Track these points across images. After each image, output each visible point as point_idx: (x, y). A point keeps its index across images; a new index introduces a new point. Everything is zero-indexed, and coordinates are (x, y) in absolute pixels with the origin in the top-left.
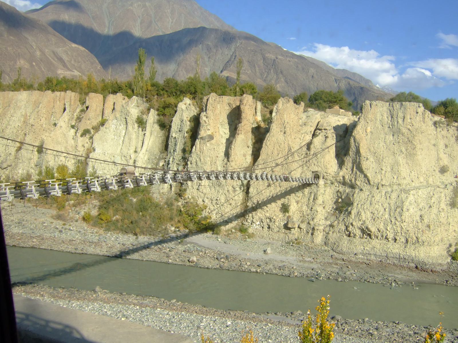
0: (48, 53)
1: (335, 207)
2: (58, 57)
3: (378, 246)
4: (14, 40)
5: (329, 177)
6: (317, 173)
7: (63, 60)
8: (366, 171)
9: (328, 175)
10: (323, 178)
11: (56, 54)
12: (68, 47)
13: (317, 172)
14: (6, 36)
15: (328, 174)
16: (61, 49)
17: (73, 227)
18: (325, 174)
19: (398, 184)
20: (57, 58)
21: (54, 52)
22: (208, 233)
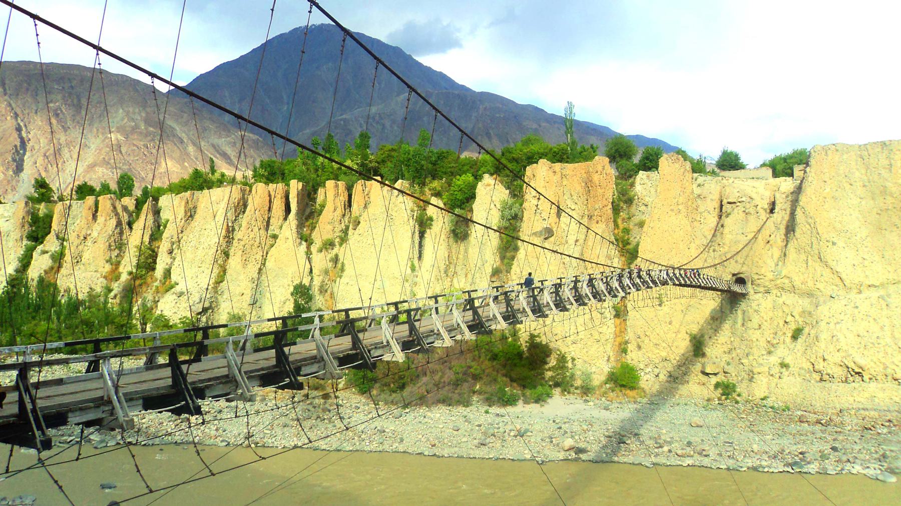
0: (205, 147)
1: (370, 503)
2: (221, 152)
3: (880, 395)
4: (155, 133)
5: (762, 281)
6: (739, 276)
7: (228, 156)
8: (833, 264)
9: (760, 277)
10: (752, 284)
11: (217, 148)
12: (233, 136)
13: (739, 273)
14: (143, 128)
15: (762, 277)
16: (223, 139)
17: (342, 400)
18: (756, 277)
19: (746, 342)
20: (220, 154)
21: (213, 146)
22: (689, 343)
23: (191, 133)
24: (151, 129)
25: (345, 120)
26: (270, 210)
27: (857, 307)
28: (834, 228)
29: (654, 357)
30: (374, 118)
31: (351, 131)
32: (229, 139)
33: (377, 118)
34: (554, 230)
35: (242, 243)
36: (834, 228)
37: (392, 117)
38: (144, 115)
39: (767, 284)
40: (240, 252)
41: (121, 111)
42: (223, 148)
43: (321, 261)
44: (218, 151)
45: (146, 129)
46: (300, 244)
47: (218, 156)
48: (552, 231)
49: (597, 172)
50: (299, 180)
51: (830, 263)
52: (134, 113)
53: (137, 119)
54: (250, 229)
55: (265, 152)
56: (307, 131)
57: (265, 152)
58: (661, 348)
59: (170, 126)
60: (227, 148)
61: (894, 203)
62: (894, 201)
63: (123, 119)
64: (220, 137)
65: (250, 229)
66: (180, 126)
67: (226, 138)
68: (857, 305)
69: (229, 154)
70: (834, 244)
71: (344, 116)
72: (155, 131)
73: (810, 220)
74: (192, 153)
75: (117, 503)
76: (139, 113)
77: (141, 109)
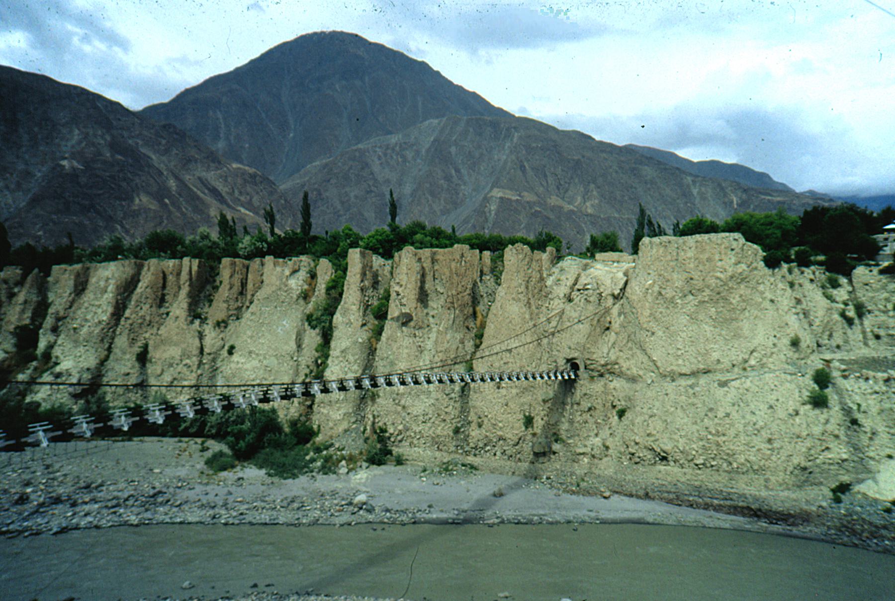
7: (219, 192)
16: (213, 172)
20: (209, 189)
23: (173, 163)
24: (119, 157)
25: (359, 150)
26: (164, 287)
27: (667, 394)
28: (655, 318)
29: (492, 436)
30: (393, 149)
31: (367, 164)
32: (219, 172)
33: (397, 148)
34: (413, 315)
35: (130, 321)
36: (655, 318)
37: (415, 147)
38: (108, 138)
39: (600, 368)
40: (127, 331)
41: (77, 132)
42: (213, 183)
43: (211, 337)
44: (205, 185)
45: (112, 156)
46: (192, 322)
47: (206, 191)
48: (411, 316)
49: (454, 260)
50: (195, 256)
51: (649, 351)
52: (95, 136)
53: (99, 144)
54: (139, 308)
55: (264, 188)
56: (317, 163)
57: (264, 188)
58: (498, 428)
59: (144, 154)
60: (218, 183)
61: (711, 295)
62: (711, 293)
63: (80, 142)
64: (208, 169)
65: (139, 308)
66: (158, 155)
67: (216, 171)
68: (668, 392)
69: (219, 189)
70: (653, 333)
71: (360, 146)
72: (123, 159)
73: (634, 310)
74: (174, 188)
75: (73, 599)
76: (102, 137)
77: (104, 131)
